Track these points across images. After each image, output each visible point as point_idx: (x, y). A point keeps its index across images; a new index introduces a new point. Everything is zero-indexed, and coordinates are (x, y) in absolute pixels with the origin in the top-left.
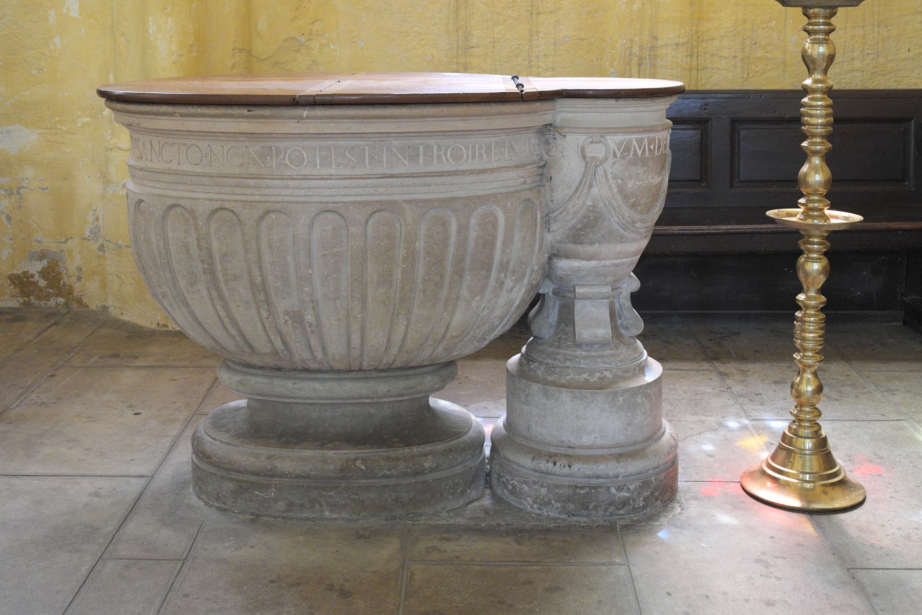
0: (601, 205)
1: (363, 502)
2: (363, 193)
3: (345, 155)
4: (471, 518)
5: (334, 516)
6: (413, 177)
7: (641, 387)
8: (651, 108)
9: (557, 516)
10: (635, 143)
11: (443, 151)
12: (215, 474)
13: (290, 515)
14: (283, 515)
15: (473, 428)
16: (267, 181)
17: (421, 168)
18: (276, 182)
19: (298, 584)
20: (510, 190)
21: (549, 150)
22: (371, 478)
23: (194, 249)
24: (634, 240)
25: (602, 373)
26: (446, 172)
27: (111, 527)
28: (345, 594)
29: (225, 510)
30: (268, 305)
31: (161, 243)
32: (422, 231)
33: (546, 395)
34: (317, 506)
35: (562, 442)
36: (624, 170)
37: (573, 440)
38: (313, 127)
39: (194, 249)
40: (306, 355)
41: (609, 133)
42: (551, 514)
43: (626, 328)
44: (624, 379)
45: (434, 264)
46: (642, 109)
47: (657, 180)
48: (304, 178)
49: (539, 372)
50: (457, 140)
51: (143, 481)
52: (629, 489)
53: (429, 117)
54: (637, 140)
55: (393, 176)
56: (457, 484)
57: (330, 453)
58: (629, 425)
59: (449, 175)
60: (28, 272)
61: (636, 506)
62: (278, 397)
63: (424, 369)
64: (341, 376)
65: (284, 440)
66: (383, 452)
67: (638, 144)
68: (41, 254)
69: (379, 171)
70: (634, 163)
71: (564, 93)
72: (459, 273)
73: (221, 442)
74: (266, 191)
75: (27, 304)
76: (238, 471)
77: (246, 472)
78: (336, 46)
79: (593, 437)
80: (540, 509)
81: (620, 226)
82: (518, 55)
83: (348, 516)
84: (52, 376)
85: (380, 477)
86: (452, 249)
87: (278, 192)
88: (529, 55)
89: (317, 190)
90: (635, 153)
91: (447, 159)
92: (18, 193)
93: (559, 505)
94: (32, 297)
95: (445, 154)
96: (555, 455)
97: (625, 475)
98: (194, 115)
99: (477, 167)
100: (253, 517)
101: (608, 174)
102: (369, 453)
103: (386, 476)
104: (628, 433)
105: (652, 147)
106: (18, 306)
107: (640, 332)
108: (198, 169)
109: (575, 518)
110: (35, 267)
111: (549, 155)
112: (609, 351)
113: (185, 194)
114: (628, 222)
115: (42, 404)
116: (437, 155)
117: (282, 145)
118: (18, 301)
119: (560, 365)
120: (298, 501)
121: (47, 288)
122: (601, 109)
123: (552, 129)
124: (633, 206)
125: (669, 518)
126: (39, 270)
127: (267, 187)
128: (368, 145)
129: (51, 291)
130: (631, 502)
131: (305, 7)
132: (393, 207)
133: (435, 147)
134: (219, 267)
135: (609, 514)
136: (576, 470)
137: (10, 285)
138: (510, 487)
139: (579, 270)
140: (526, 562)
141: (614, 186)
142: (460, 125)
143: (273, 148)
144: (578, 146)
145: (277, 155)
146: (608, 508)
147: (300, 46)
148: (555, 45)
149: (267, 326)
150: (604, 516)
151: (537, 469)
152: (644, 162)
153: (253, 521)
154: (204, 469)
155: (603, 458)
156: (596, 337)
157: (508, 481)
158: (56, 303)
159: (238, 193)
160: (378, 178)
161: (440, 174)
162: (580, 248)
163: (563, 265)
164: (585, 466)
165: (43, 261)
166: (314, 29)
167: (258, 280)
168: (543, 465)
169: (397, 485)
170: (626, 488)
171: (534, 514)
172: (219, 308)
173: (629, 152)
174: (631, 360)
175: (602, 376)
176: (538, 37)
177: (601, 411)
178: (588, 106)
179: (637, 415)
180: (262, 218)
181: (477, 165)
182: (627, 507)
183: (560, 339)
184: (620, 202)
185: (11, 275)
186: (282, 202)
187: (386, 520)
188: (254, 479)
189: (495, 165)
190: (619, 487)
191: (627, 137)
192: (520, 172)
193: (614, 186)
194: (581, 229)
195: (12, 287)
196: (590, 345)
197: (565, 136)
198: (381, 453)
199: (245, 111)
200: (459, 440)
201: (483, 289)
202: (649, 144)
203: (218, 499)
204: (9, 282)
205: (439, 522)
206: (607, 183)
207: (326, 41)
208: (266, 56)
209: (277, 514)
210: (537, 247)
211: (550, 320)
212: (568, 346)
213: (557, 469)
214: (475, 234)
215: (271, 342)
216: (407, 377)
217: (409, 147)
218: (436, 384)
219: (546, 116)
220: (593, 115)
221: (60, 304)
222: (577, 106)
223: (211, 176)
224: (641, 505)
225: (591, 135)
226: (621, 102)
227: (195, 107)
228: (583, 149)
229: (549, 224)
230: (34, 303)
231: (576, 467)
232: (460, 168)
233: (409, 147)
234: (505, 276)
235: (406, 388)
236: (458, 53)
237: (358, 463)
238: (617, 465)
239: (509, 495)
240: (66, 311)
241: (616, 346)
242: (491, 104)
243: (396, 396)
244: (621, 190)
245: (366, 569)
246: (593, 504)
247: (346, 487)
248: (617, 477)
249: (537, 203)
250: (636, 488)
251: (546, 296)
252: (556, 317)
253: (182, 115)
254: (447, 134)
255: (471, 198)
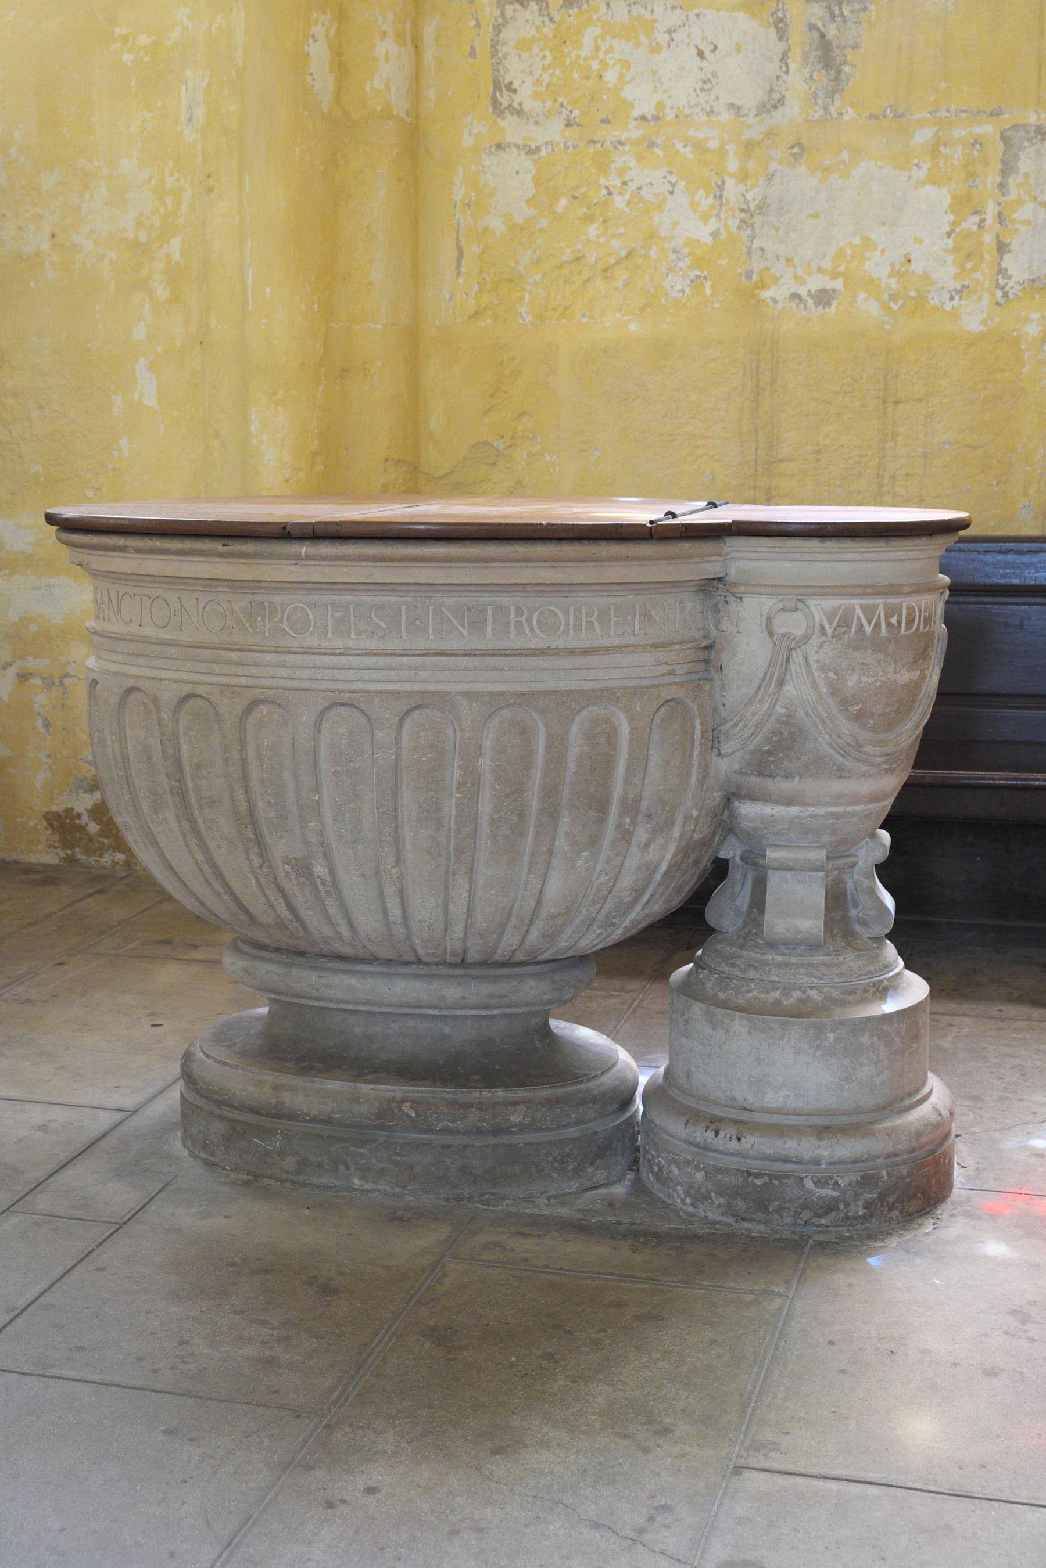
0: (800, 713)
1: (411, 1167)
2: (397, 678)
3: (371, 618)
4: (580, 1210)
5: (367, 1186)
6: (475, 655)
7: (869, 1019)
8: (893, 555)
9: (721, 1218)
10: (859, 612)
11: (525, 616)
12: (201, 1109)
13: (302, 1178)
14: (293, 1178)
15: (615, 1069)
16: (256, 655)
17: (490, 641)
18: (268, 657)
19: (268, 1271)
20: (644, 683)
21: (719, 622)
22: (425, 1132)
23: (157, 757)
24: (864, 775)
25: (804, 992)
26: (529, 649)
27: (40, 1173)
28: (328, 1290)
29: (213, 1164)
30: (260, 848)
31: (117, 746)
32: (488, 744)
33: (712, 1022)
34: (342, 1167)
35: (734, 1099)
36: (840, 657)
37: (750, 1098)
38: (316, 573)
39: (157, 757)
40: (327, 931)
41: (811, 595)
42: (710, 1216)
43: (863, 923)
44: (843, 1003)
45: (507, 796)
46: (871, 555)
47: (906, 676)
48: (307, 652)
49: (709, 985)
50: (549, 599)
51: (118, 1117)
52: (836, 1184)
53: (494, 560)
54: (864, 608)
55: (441, 653)
56: (568, 1156)
57: (365, 1088)
58: (847, 1079)
59: (534, 655)
60: (72, 809)
61: (850, 1214)
62: (297, 995)
63: (526, 968)
64: (392, 970)
65: (306, 1063)
66: (448, 1093)
67: (864, 613)
68: (92, 783)
69: (421, 644)
70: (857, 645)
71: (734, 528)
72: (551, 813)
73: (214, 1061)
74: (254, 671)
75: (71, 860)
76: (232, 1106)
77: (241, 1107)
78: (555, 457)
79: (782, 1094)
80: (694, 1207)
81: (835, 750)
82: (859, 475)
83: (387, 1188)
84: (60, 964)
85: (436, 1131)
86: (538, 773)
87: (271, 671)
88: (878, 475)
89: (327, 671)
90: (860, 627)
91: (532, 630)
92: (61, 684)
93: (722, 1201)
94: (77, 850)
95: (529, 620)
96: (720, 1120)
97: (831, 1160)
98: (152, 551)
99: (588, 644)
100: (250, 1178)
101: (811, 663)
102: (425, 1092)
103: (447, 1131)
104: (845, 1094)
105: (894, 620)
106: (57, 862)
107: (887, 931)
108: (165, 635)
109: (746, 1225)
110: (83, 803)
111: (718, 630)
112: (821, 958)
113: (148, 672)
114: (848, 744)
115: (28, 1001)
116: (516, 622)
117: (278, 599)
118: (57, 854)
119: (740, 975)
120: (314, 1159)
121: (100, 836)
122: (798, 556)
123: (721, 586)
124: (858, 717)
125: (905, 1239)
126: (89, 807)
127: (256, 665)
128: (405, 604)
129: (106, 841)
130: (842, 1206)
131: (505, 392)
132: (443, 701)
133: (513, 609)
134: (190, 785)
135: (802, 1222)
136: (749, 1146)
137: (46, 829)
138: (656, 1169)
139: (772, 820)
140: (631, 1276)
141: (821, 683)
142: (547, 575)
143: (266, 604)
144: (762, 616)
145: (272, 616)
146: (801, 1213)
147: (497, 456)
148: (925, 455)
149: (262, 880)
150: (793, 1224)
151: (691, 1140)
152: (877, 644)
153: (247, 1184)
154: (190, 1100)
155: (795, 1131)
156: (798, 932)
157: (654, 1158)
158: (113, 861)
159: (217, 672)
160: (419, 655)
161: (519, 653)
162: (769, 784)
163: (748, 810)
164: (763, 1140)
165: (94, 793)
166: (520, 428)
167: (243, 807)
168: (702, 1135)
169: (466, 1146)
170: (831, 1182)
171: (685, 1213)
172: (194, 848)
173: (849, 627)
174: (861, 975)
175: (804, 996)
176: (896, 442)
177: (797, 1053)
178: (777, 550)
179: (862, 1064)
180: (248, 710)
181: (585, 641)
182: (833, 1213)
183: (748, 934)
184: (834, 711)
185: (47, 813)
186: (277, 689)
187: (447, 1200)
188: (252, 1118)
189: (616, 641)
190: (819, 1180)
191: (846, 602)
192: (661, 655)
193: (821, 683)
194: (769, 753)
195: (49, 832)
196: (790, 944)
197: (741, 599)
198: (445, 1095)
199: (217, 546)
200: (579, 1087)
201: (594, 841)
202: (888, 616)
203: (205, 1147)
204: (45, 823)
205: (527, 1211)
206: (808, 677)
207: (538, 448)
208: (441, 473)
209: (284, 1176)
210: (694, 778)
211: (738, 902)
212: (757, 946)
213: (720, 1142)
214: (577, 750)
215: (272, 906)
216: (496, 979)
217: (469, 609)
218: (545, 993)
219: (707, 565)
220: (787, 564)
221: (117, 863)
222: (759, 549)
223: (181, 646)
224: (860, 1213)
225: (781, 597)
226: (831, 544)
227: (154, 538)
228: (769, 620)
229: (719, 742)
230: (79, 860)
231: (750, 1141)
232: (554, 645)
233: (469, 609)
234: (634, 823)
235: (491, 996)
236: (756, 471)
237: (406, 1107)
238: (817, 1143)
239: (654, 1182)
240: (125, 874)
241: (838, 951)
242: (600, 542)
243: (477, 1008)
244: (835, 690)
245: (378, 1263)
246: (776, 1203)
247: (385, 1142)
248: (817, 1162)
249: (694, 707)
250: (850, 1184)
251: (730, 864)
252: (748, 896)
253: (138, 551)
254: (529, 588)
255: (570, 693)
